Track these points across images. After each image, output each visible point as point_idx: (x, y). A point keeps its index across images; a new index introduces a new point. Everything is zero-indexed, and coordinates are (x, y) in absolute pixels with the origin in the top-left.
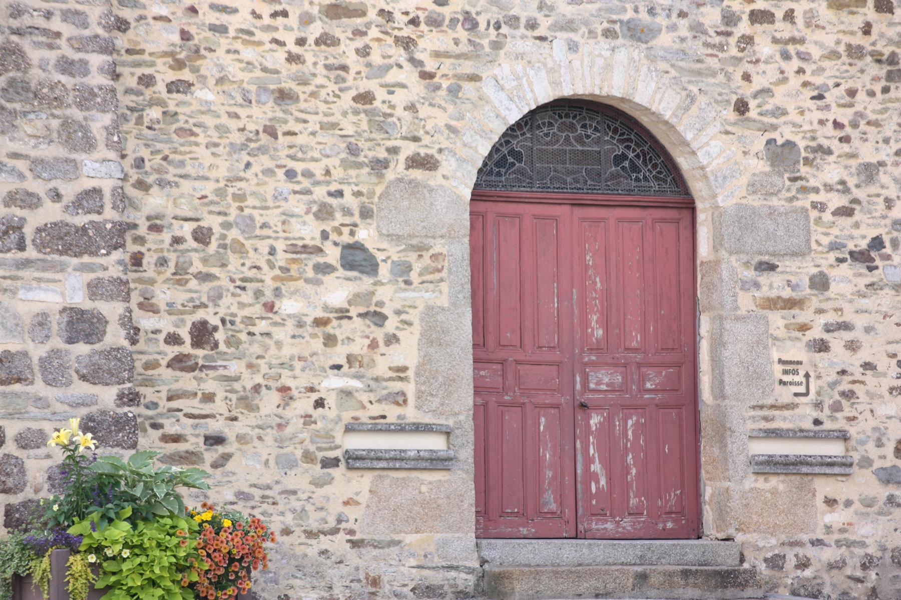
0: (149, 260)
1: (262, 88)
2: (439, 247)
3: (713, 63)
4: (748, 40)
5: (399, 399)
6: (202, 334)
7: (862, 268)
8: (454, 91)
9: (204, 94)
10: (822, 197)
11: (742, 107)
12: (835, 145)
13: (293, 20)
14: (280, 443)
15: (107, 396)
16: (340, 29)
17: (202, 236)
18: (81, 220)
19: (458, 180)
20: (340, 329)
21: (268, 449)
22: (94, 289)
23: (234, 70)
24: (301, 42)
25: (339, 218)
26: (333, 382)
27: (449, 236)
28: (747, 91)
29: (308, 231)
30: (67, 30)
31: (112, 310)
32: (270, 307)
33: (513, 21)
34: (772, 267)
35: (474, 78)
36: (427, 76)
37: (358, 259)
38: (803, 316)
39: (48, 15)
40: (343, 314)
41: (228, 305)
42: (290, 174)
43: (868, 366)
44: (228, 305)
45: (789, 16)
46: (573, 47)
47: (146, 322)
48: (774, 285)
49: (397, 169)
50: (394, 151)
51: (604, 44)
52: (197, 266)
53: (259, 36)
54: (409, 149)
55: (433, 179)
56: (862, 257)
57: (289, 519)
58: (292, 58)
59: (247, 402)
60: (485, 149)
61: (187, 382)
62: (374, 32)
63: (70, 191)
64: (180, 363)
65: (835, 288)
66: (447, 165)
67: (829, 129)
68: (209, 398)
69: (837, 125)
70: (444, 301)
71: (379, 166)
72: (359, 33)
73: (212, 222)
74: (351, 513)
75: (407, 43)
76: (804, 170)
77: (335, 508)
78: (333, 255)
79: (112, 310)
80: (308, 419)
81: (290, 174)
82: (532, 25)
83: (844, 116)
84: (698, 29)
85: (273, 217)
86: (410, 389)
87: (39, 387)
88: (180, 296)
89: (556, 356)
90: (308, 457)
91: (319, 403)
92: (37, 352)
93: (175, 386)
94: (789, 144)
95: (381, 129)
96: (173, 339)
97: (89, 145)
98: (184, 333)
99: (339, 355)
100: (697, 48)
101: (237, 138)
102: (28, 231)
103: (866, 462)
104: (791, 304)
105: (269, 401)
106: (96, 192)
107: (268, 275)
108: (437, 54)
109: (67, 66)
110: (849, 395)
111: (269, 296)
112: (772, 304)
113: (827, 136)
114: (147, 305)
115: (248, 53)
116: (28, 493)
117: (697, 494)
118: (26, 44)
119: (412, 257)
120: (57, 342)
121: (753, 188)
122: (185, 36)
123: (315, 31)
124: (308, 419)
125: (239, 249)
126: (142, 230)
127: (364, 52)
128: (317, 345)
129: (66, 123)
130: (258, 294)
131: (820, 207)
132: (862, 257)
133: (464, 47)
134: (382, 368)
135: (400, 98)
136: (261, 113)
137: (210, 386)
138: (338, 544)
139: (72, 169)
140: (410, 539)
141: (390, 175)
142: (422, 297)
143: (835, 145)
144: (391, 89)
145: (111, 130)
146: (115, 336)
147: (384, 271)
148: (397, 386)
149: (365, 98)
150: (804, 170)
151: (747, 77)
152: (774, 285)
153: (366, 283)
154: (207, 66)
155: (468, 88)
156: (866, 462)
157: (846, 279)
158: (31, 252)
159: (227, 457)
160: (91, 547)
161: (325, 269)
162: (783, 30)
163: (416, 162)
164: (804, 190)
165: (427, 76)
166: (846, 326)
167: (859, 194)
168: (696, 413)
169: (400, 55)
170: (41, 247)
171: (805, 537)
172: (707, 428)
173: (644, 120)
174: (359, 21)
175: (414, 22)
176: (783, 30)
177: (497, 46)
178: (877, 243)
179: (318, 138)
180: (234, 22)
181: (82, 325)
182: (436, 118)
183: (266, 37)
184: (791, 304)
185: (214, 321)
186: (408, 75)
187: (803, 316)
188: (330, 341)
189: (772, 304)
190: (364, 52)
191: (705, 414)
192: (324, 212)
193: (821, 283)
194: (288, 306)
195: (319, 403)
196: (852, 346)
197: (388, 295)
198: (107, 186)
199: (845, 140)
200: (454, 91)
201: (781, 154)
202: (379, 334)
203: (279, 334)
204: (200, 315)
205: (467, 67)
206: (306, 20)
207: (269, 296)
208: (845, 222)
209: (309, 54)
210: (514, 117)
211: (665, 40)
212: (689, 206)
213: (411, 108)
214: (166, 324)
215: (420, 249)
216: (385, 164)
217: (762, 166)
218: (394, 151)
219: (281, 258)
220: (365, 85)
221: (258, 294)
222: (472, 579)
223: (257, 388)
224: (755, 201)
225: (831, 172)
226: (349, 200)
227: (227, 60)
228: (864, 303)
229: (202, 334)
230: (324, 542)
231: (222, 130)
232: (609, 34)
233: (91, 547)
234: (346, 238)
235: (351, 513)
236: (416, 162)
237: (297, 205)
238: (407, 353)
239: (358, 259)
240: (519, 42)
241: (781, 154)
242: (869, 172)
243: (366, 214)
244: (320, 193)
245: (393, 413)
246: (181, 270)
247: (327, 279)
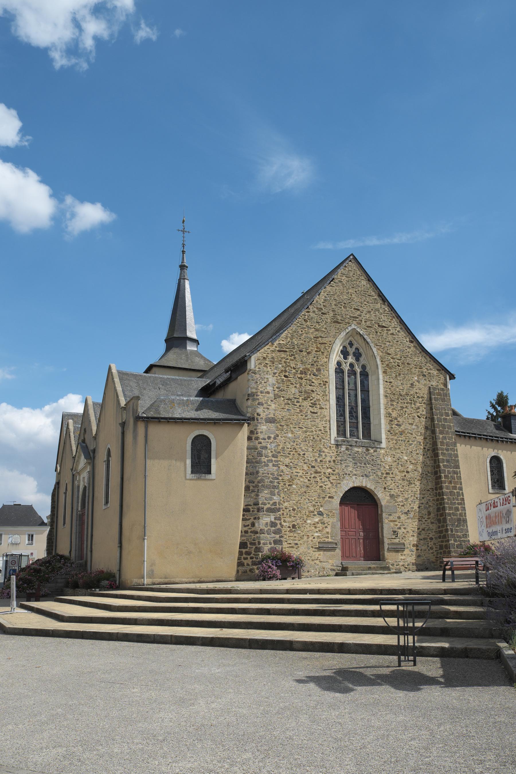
0: (285, 514)
1: (304, 485)
2: (334, 511)
3: (380, 481)
4: (385, 477)
5: (328, 537)
6: (294, 526)
7: (406, 515)
8: (336, 486)
9: (294, 486)
10: (399, 503)
11: (385, 488)
12: (401, 495)
13: (309, 474)
14: (307, 545)
15: (277, 536)
16: (317, 475)
17: (294, 510)
18: (273, 507)
19: (337, 500)
20: (318, 525)
21: (305, 545)
22: (275, 519)
23: (299, 483)
24: (310, 478)
25: (317, 507)
26: (316, 534)
27: (335, 510)
28: (386, 486)
29: (312, 509)
30: (271, 476)
31: (278, 522)
32: (305, 522)
33: (346, 474)
34: (391, 515)
35: (339, 483)
36: (331, 483)
37: (321, 514)
38: (397, 523)
39: (268, 474)
40: (318, 523)
41: (298, 521)
42: (309, 499)
43: (407, 532)
44: (298, 521)
45: (392, 473)
46: (356, 478)
47: (284, 524)
48: (391, 518)
49: (327, 498)
50: (326, 495)
51: (361, 478)
52: (293, 515)
53: (304, 477)
54: (329, 495)
55: (333, 500)
56: (406, 513)
57: (309, 558)
58: (309, 480)
59: (302, 538)
60: (342, 495)
61: (292, 534)
62: (322, 476)
63: (271, 502)
64: (290, 531)
65: (402, 518)
66: (335, 498)
67: (400, 492)
68: (295, 537)
69: (401, 491)
70: (335, 521)
71: (324, 498)
72: (320, 476)
73: (296, 507)
74: (320, 557)
75: (328, 478)
76: (396, 499)
77: (317, 556)
78: (316, 513)
79: (278, 522)
80: (312, 541)
81: (309, 499)
82: (349, 475)
83: (402, 490)
84: (377, 475)
85: (306, 507)
86: (329, 535)
87: (266, 535)
88: (290, 520)
89: (354, 530)
90: (312, 547)
91: (314, 538)
92: (266, 529)
93: (290, 535)
94: (393, 495)
95: (324, 492)
96: (289, 527)
97: (274, 495)
98: (291, 526)
99: (317, 530)
100: (377, 479)
101: (300, 493)
102: (265, 509)
103: (408, 548)
104: (394, 521)
105: (305, 538)
106: (276, 502)
107: (305, 516)
108: (333, 480)
109: (271, 482)
110: (404, 537)
111: (305, 520)
112: (391, 521)
113: (399, 493)
114: (285, 521)
115: (301, 479)
116: (265, 552)
117: (379, 553)
118: (265, 478)
119: (329, 513)
120: (269, 527)
121: (387, 502)
122: (291, 477)
123: (313, 476)
124: (312, 541)
125: (300, 512)
126: (284, 509)
127: (321, 479)
128: (313, 528)
129: (271, 491)
130: (303, 519)
131: (399, 505)
132: (406, 513)
133: (338, 478)
134: (325, 532)
135: (327, 487)
136: (303, 490)
137: (295, 535)
138: (317, 562)
139: (271, 499)
140: (330, 561)
141: (326, 499)
142: (331, 520)
143: (401, 495)
144: (325, 485)
145: (278, 492)
146: (279, 526)
147: (325, 516)
148: (327, 535)
149: (321, 487)
150: (396, 499)
151: (386, 483)
152: (391, 518)
153: (322, 517)
154: (295, 481)
155: (339, 485)
156: (408, 548)
157: (403, 517)
158: (265, 512)
159: (298, 547)
160: (68, 583)
161: (315, 515)
162: (391, 476)
163: (330, 497)
164: (396, 502)
165: (331, 483)
166: (404, 525)
167: (405, 503)
168: (379, 539)
169: (327, 479)
170: (267, 511)
171: (398, 561)
172: (381, 543)
173: (369, 490)
174: (320, 474)
175: (329, 474)
176: (391, 476)
177: (343, 478)
178: (408, 511)
179: (314, 493)
180: (299, 474)
181: (273, 524)
182: (333, 490)
183: (304, 477)
184: (394, 521)
185: (296, 524)
186: (328, 483)
187: (397, 523)
188: (315, 527)
189: (391, 521)
190: (321, 479)
191: (380, 540)
192: (314, 506)
193: (399, 518)
194: (309, 521)
195: (314, 538)
196: (405, 528)
197: (326, 520)
198: (277, 501)
199: (402, 494)
200: (336, 486)
201: (392, 496)
202: (324, 526)
203: (307, 526)
204: (294, 523)
205: (339, 481)
206: (311, 474)
207: (305, 520)
208: (403, 508)
209: (312, 479)
210: (346, 490)
211: (371, 477)
212: (377, 505)
213: (329, 488)
214: (288, 524)
215: (331, 512)
216: (325, 498)
217: (389, 498)
218: (326, 495)
219: (307, 513)
220: (321, 485)
221: (303, 519)
222: (341, 568)
223: (303, 535)
224: (388, 504)
225: (400, 499)
226: (319, 504)
227: (298, 481)
228: (407, 521)
229: (294, 526)
230: (315, 561)
231: (297, 492)
232: (362, 476)
233: (68, 583)
234: (318, 510)
235: (320, 557)
236: (330, 497)
237: (310, 504)
238: (328, 530)
239: (321, 514)
240: (347, 477)
241: (392, 496)
242: (407, 499)
243: (322, 506)
244: (314, 502)
245: (327, 540)
246: (290, 515)
247: (315, 517)
